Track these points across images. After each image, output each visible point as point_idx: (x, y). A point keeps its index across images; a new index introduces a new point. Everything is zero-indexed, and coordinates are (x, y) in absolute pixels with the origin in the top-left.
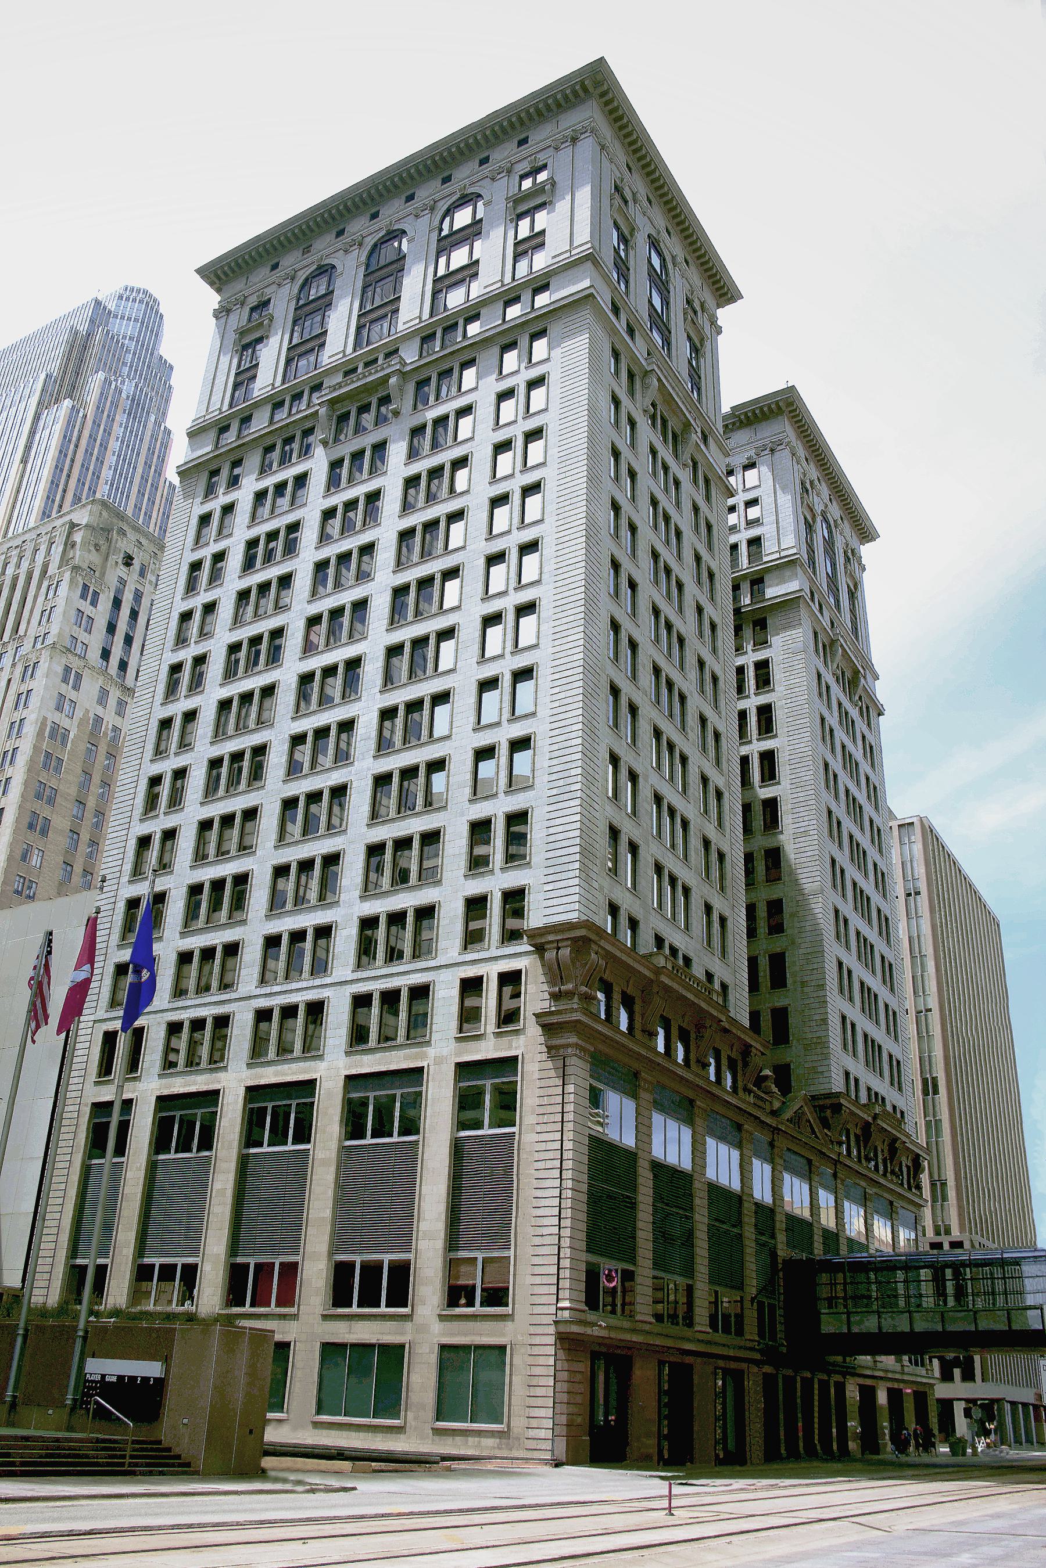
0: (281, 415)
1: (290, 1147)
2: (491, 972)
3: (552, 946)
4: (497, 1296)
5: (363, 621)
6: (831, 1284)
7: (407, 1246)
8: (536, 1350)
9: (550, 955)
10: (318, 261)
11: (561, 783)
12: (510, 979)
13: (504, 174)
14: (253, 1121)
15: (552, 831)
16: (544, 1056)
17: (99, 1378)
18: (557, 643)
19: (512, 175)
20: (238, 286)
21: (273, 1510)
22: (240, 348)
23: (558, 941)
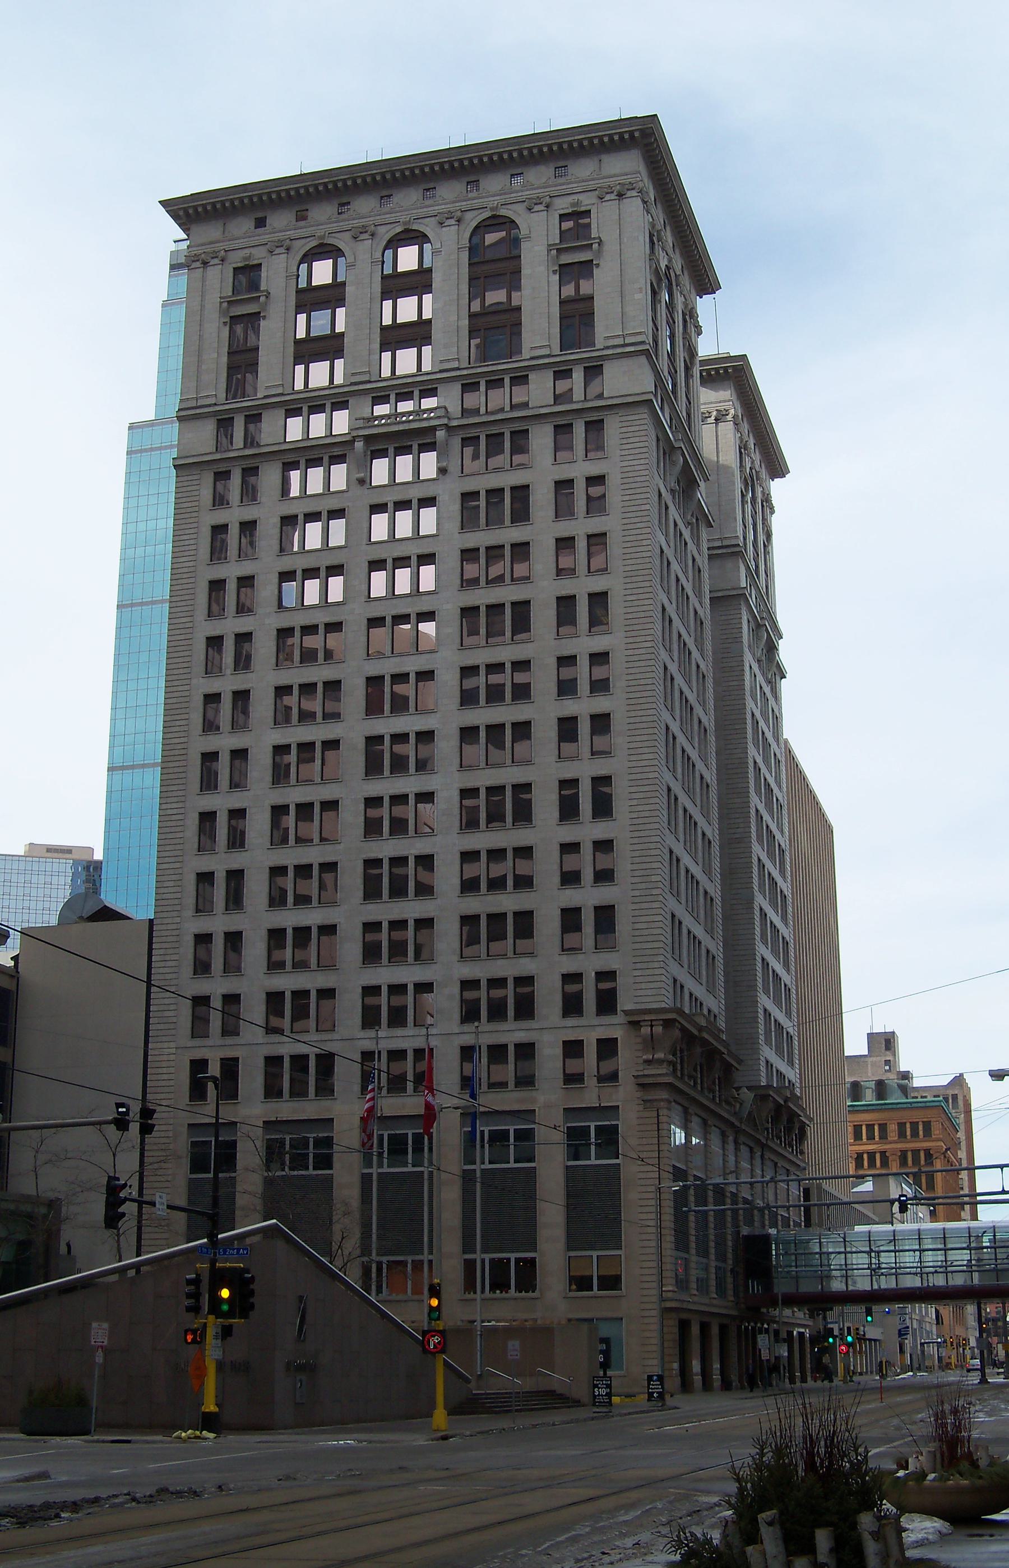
0: (472, 400)
1: (410, 1169)
2: (590, 1039)
3: (646, 1023)
4: (611, 1282)
5: (245, 712)
6: (896, 1274)
7: (533, 1247)
8: (646, 1321)
9: (645, 1030)
10: (323, 237)
11: (644, 886)
12: (607, 1047)
13: (613, 196)
14: (273, 1152)
15: (637, 926)
16: (641, 1108)
17: (875, 1308)
18: (633, 758)
19: (463, 226)
20: (210, 232)
21: (270, 1442)
22: (228, 320)
23: (651, 1021)
